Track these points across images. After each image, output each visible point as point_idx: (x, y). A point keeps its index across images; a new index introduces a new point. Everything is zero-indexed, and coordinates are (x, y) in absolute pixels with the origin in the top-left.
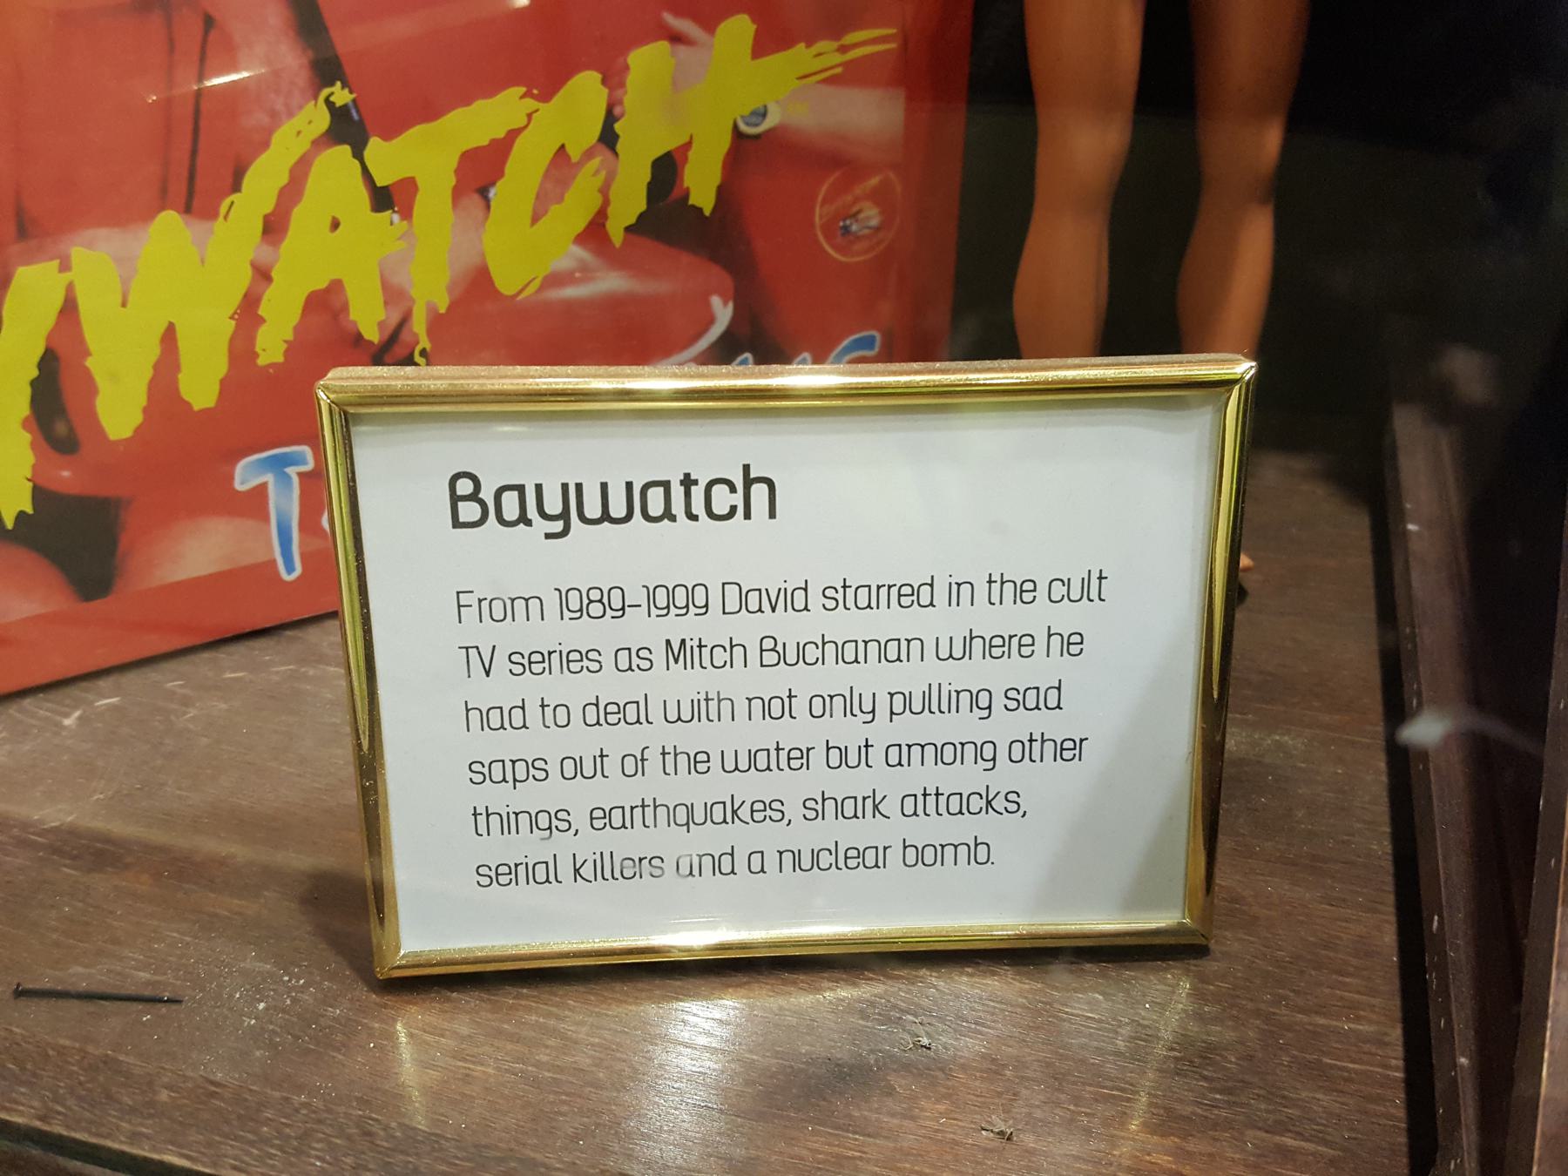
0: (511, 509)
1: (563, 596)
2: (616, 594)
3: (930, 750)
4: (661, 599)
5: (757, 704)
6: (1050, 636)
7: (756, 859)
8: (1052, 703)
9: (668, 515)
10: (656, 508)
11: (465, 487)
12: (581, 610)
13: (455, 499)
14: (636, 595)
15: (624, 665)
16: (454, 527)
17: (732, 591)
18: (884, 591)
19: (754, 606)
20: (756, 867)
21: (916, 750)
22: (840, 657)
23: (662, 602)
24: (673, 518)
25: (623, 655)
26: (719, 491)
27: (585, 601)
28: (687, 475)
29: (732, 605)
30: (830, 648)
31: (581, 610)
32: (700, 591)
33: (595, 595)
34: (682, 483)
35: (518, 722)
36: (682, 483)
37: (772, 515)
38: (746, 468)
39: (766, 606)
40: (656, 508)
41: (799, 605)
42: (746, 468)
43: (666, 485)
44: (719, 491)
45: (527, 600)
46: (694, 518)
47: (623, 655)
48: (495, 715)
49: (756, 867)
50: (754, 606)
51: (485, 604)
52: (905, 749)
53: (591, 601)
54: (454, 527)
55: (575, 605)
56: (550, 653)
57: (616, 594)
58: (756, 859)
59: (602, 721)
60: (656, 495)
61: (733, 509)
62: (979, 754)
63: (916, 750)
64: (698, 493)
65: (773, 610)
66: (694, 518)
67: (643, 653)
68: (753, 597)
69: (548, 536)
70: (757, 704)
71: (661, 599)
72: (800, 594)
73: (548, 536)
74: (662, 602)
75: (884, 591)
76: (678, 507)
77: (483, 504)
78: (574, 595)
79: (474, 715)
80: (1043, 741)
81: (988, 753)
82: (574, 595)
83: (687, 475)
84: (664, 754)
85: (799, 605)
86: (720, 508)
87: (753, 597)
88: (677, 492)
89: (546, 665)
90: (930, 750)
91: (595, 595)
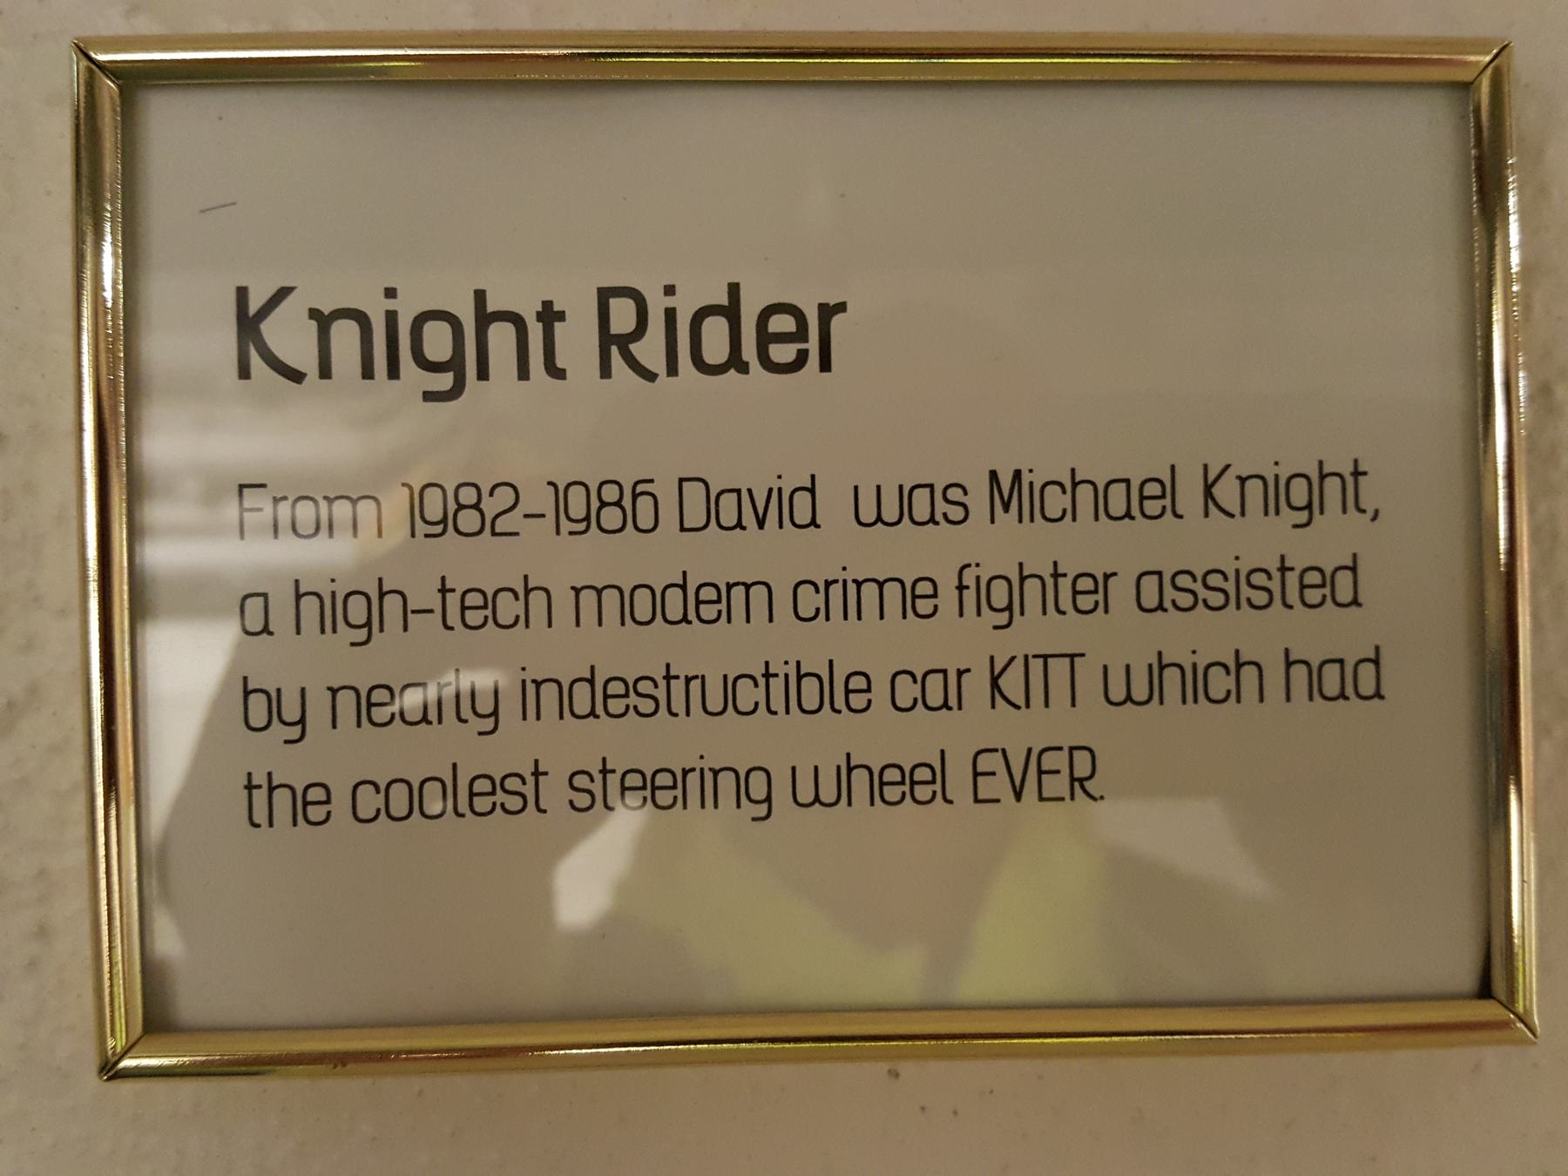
0: (716, 343)
1: (560, 493)
5: (346, 699)
6: (298, 597)
8: (1367, 687)
9: (736, 362)
12: (587, 518)
14: (539, 499)
15: (1150, 600)
17: (694, 492)
19: (729, 518)
24: (743, 368)
25: (1150, 583)
27: (595, 504)
28: (547, 305)
29: (695, 517)
31: (587, 518)
33: (610, 493)
34: (540, 317)
35: (1367, 687)
36: (540, 317)
38: (480, 296)
39: (749, 519)
41: (803, 516)
42: (480, 296)
47: (1150, 583)
48: (1332, 672)
50: (729, 518)
53: (461, 507)
55: (578, 510)
59: (599, 710)
62: (742, 791)
65: (761, 524)
67: (955, 494)
68: (729, 501)
69: (429, 396)
70: (346, 699)
72: (803, 499)
73: (429, 396)
78: (577, 495)
79: (1299, 672)
80: (271, 789)
81: (758, 791)
82: (577, 495)
83: (547, 305)
85: (803, 516)
87: (729, 501)
89: (1100, 597)
91: (610, 493)
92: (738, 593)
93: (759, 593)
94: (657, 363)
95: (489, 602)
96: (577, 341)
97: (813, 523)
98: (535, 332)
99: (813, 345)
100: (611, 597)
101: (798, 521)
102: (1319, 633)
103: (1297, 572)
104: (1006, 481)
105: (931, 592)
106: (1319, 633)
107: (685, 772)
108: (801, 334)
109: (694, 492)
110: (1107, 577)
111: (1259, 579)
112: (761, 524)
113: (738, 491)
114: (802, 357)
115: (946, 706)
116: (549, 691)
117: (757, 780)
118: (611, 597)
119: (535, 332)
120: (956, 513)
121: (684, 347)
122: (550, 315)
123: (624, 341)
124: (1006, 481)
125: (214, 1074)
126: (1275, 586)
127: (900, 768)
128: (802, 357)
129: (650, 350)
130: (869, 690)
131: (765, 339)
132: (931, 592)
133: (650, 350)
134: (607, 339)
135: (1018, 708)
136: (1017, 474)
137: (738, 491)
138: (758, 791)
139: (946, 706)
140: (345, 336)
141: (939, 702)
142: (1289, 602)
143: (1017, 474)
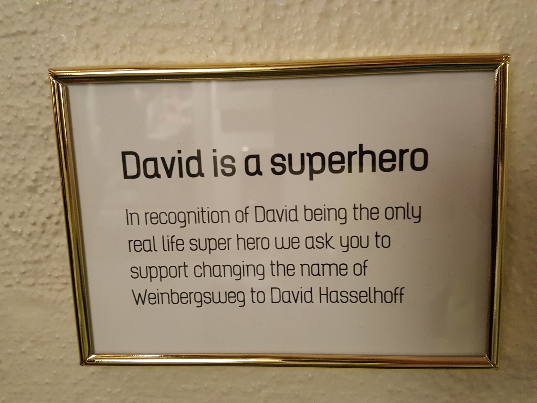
3: (333, 268)
5: (305, 268)
7: (252, 163)
10: (151, 172)
15: (309, 245)
16: (258, 155)
17: (260, 211)
20: (252, 168)
21: (327, 267)
22: (212, 273)
25: (309, 240)
30: (207, 269)
40: (151, 172)
45: (330, 265)
47: (309, 240)
49: (252, 168)
52: (321, 266)
54: (258, 155)
56: (257, 239)
58: (252, 163)
63: (327, 267)
65: (280, 220)
68: (270, 213)
70: (305, 268)
84: (272, 265)
85: (308, 299)
87: (270, 213)
90: (333, 268)
95: (142, 244)
97: (296, 220)
99: (397, 163)
101: (291, 219)
102: (144, 260)
103: (133, 242)
105: (297, 241)
106: (144, 260)
107: (190, 293)
108: (394, 159)
109: (260, 210)
110: (228, 239)
111: (320, 240)
112: (280, 220)
113: (273, 210)
114: (394, 166)
115: (319, 274)
116: (251, 268)
125: (440, 356)
127: (234, 293)
128: (394, 166)
130: (294, 269)
132: (297, 241)
137: (273, 210)
139: (319, 274)
141: (317, 273)
142: (378, 246)
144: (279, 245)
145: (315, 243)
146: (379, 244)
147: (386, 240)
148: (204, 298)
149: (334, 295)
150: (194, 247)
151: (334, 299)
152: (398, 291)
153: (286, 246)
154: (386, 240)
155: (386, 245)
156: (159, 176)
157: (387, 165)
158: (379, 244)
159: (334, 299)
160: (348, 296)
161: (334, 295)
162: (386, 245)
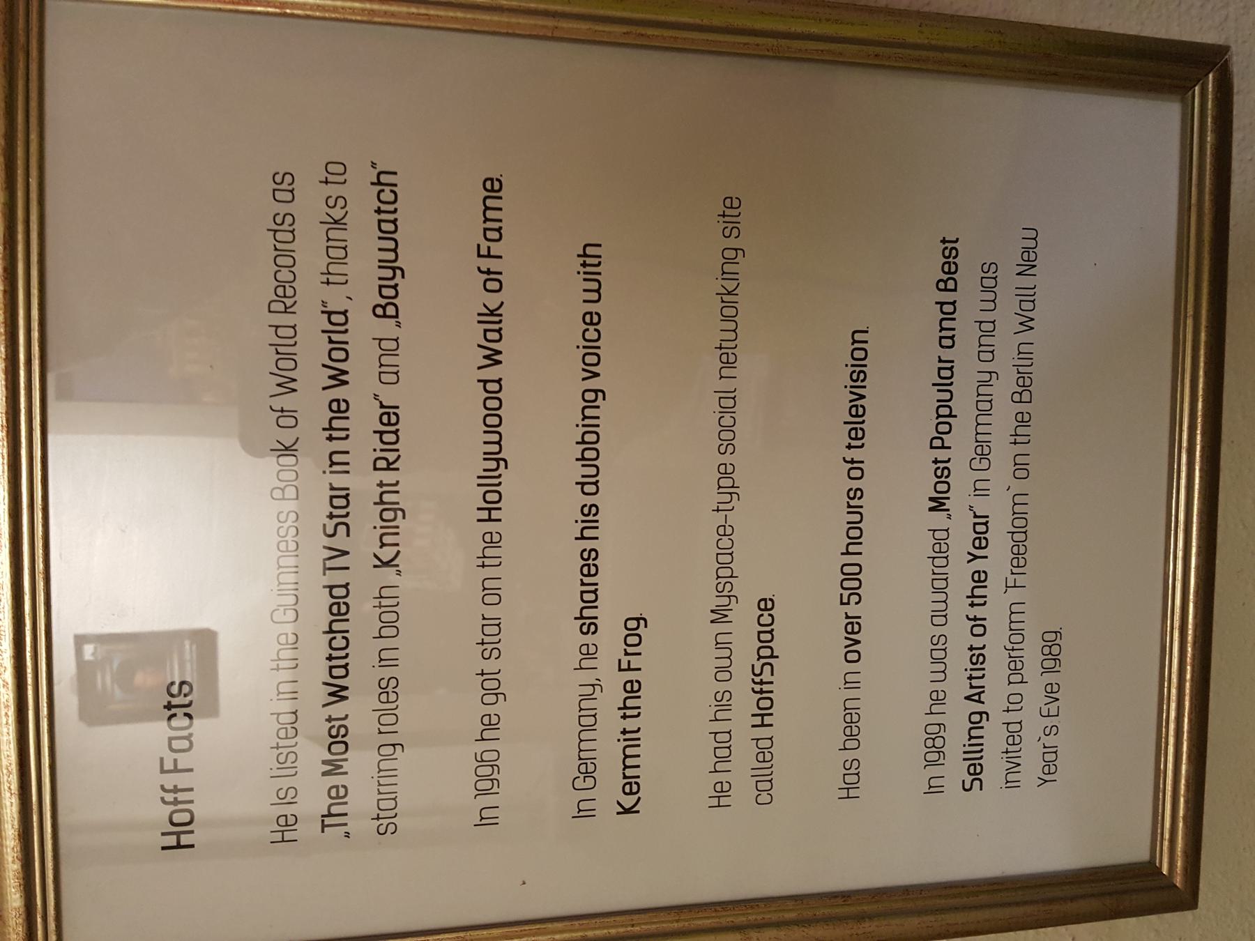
2: (1047, 637)
4: (486, 785)
9: (396, 432)
11: (379, 311)
13: (385, 316)
15: (288, 196)
18: (382, 789)
23: (488, 784)
25: (279, 195)
26: (335, 644)
32: (393, 631)
33: (930, 743)
37: (395, 173)
38: (375, 504)
43: (331, 668)
44: (335, 644)
46: (396, 210)
47: (279, 195)
51: (630, 650)
57: (1047, 637)
60: (385, 226)
61: (392, 191)
64: (384, 207)
66: (396, 210)
67: (278, 179)
71: (486, 785)
74: (488, 784)
75: (382, 789)
76: (391, 217)
77: (388, 304)
78: (1046, 664)
81: (732, 254)
82: (1046, 664)
86: (391, 198)
88: (334, 662)
91: (1046, 650)
92: (980, 438)
93: (595, 296)
94: (396, 454)
96: (389, 477)
98: (385, 489)
100: (584, 736)
104: (716, 616)
114: (395, 414)
117: (728, 254)
118: (584, 736)
119: (385, 489)
120: (727, 695)
121: (392, 447)
122: (381, 485)
123: (389, 464)
124: (716, 616)
126: (490, 647)
128: (395, 414)
129: (391, 456)
131: (389, 424)
133: (391, 456)
134: (388, 469)
135: (398, 552)
136: (712, 611)
138: (732, 254)
140: (386, 540)
143: (712, 611)
144: (595, 296)
145: (285, 227)
146: (341, 179)
147: (1012, 699)
148: (725, 593)
149: (849, 779)
150: (730, 449)
151: (854, 779)
152: (169, 797)
153: (733, 326)
154: (1012, 699)
155: (340, 169)
156: (191, 735)
157: (393, 419)
158: (341, 179)
159: (854, 779)
160: (286, 525)
161: (849, 779)
162: (340, 169)
